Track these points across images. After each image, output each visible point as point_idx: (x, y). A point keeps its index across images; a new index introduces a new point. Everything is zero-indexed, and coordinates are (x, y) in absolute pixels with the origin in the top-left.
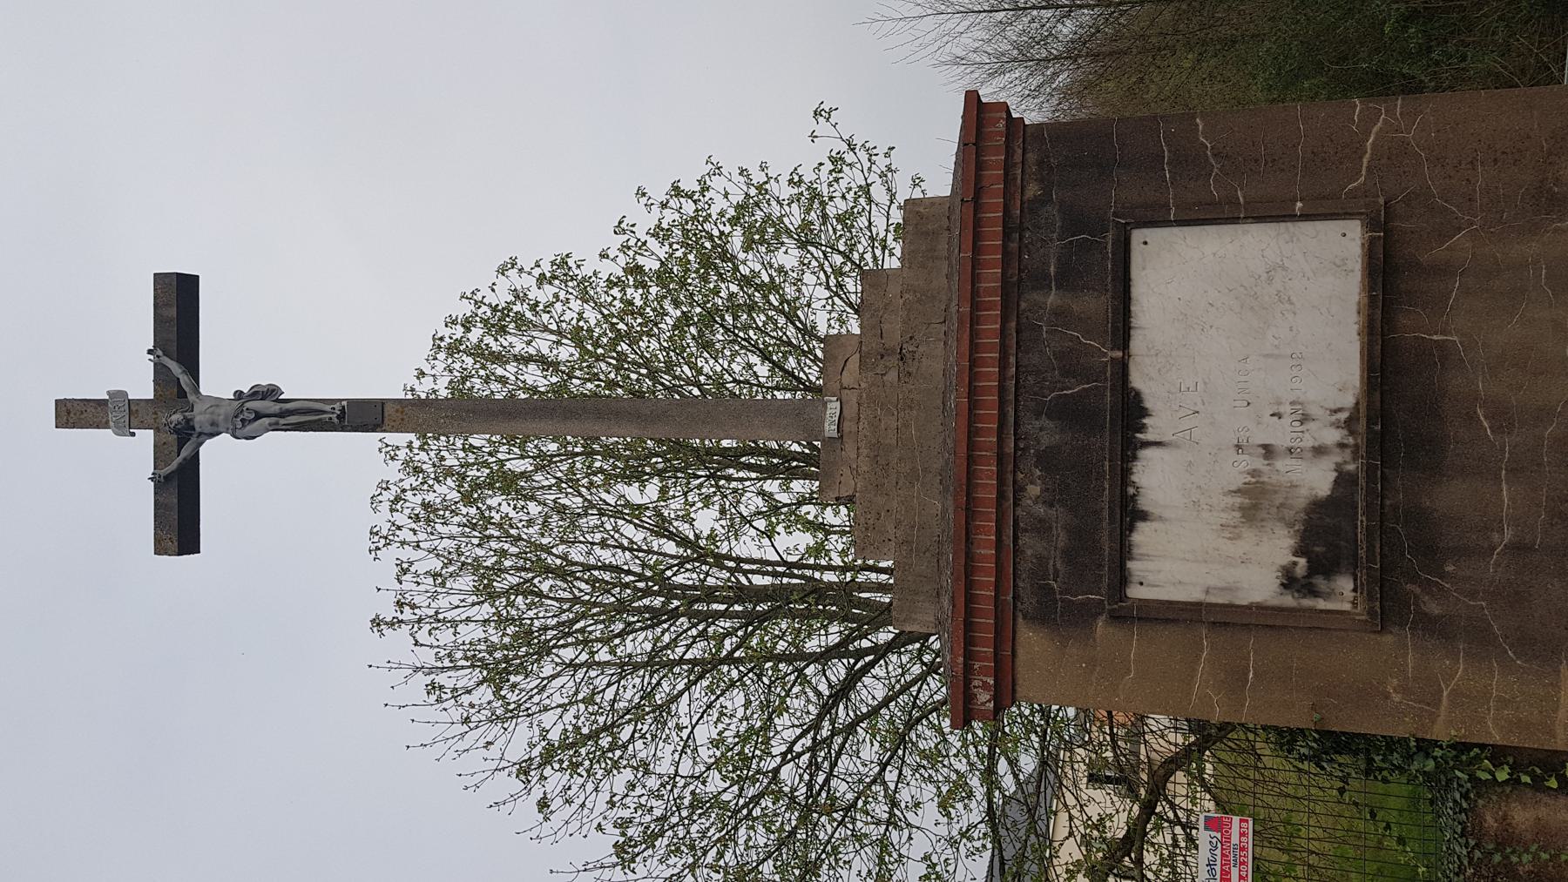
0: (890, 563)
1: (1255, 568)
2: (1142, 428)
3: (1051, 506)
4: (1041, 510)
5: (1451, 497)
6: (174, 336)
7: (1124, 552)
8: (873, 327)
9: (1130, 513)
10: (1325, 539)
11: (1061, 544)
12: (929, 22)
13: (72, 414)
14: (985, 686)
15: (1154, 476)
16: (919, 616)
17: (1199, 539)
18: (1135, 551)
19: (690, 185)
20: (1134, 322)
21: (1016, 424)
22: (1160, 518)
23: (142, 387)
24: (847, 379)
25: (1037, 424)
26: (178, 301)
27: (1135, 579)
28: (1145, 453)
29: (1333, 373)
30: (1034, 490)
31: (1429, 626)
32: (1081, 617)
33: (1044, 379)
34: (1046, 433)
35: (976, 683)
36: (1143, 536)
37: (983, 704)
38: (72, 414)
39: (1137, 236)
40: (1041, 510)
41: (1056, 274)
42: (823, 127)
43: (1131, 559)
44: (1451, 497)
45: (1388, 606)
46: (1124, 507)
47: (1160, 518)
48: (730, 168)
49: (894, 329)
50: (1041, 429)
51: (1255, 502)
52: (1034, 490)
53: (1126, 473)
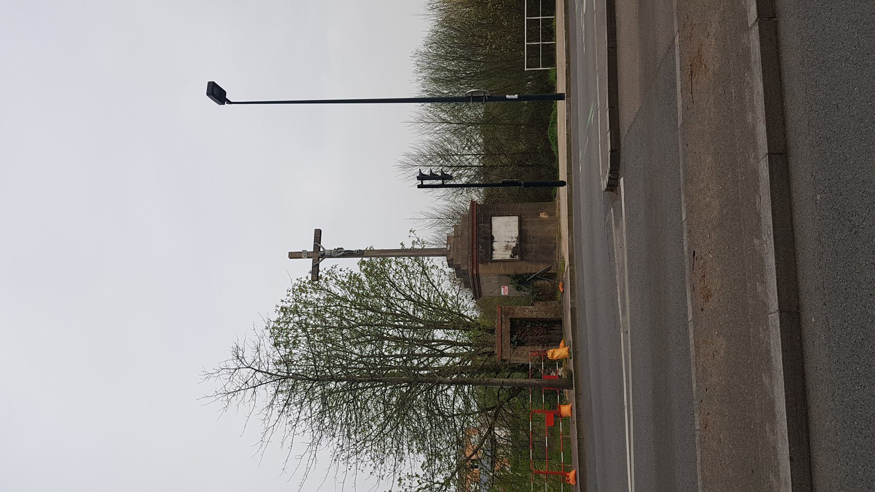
0: (516, 96)
1: (507, 255)
5: (529, 246)
7: (492, 254)
10: (515, 251)
12: (428, 221)
13: (293, 255)
15: (495, 245)
17: (500, 252)
23: (310, 249)
26: (318, 234)
29: (515, 233)
31: (526, 260)
32: (487, 262)
34: (482, 241)
36: (494, 252)
38: (293, 255)
44: (529, 246)
45: (522, 259)
49: (460, 233)
51: (507, 248)
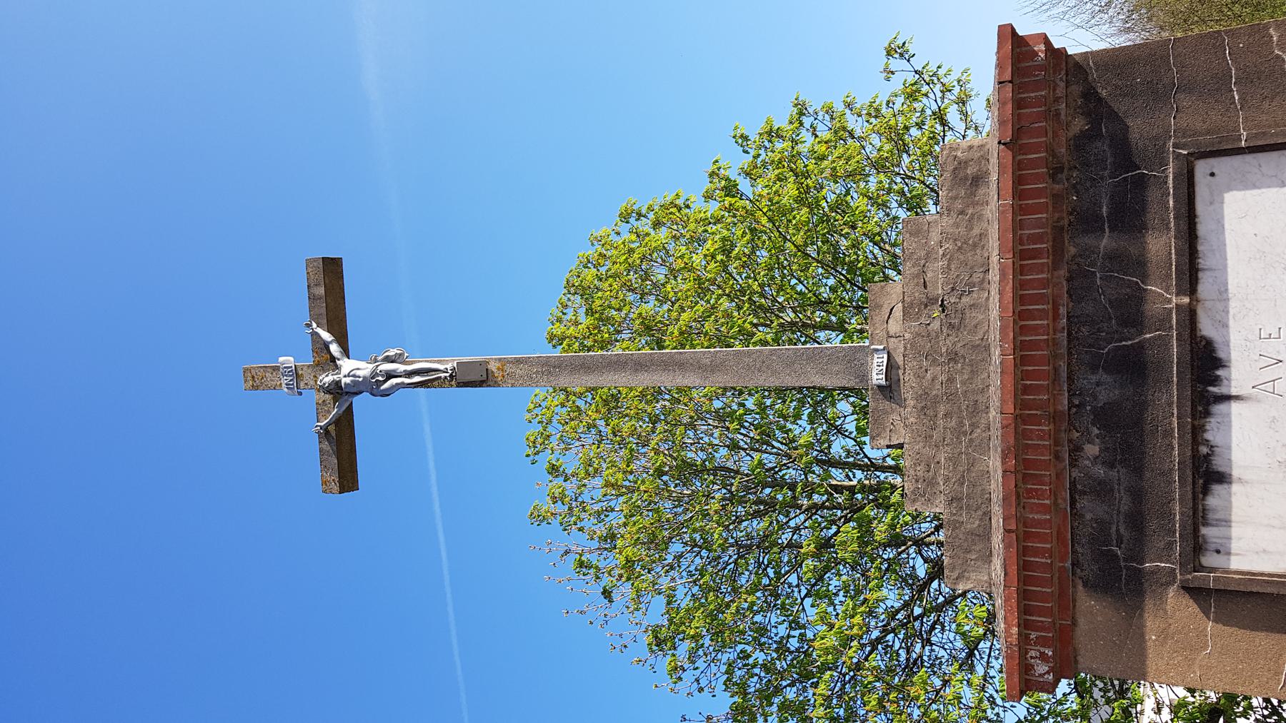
2: (1216, 381)
3: (1112, 466)
4: (1100, 471)
6: (323, 311)
7: (1198, 517)
8: (917, 276)
9: (1207, 474)
11: (1124, 508)
14: (1043, 657)
16: (973, 576)
18: (1211, 516)
19: (782, 123)
20: (1202, 263)
21: (1070, 379)
22: (1210, 270)
24: (894, 327)
25: (1094, 378)
27: (1213, 547)
28: (1219, 408)
30: (1092, 450)
33: (1099, 330)
35: (1033, 653)
37: (1041, 675)
39: (1202, 168)
40: (1100, 471)
41: (1110, 214)
42: (896, 64)
43: (1206, 524)
46: (1196, 469)
47: (1210, 270)
48: (814, 104)
50: (1098, 384)
52: (1092, 450)
53: (1196, 434)
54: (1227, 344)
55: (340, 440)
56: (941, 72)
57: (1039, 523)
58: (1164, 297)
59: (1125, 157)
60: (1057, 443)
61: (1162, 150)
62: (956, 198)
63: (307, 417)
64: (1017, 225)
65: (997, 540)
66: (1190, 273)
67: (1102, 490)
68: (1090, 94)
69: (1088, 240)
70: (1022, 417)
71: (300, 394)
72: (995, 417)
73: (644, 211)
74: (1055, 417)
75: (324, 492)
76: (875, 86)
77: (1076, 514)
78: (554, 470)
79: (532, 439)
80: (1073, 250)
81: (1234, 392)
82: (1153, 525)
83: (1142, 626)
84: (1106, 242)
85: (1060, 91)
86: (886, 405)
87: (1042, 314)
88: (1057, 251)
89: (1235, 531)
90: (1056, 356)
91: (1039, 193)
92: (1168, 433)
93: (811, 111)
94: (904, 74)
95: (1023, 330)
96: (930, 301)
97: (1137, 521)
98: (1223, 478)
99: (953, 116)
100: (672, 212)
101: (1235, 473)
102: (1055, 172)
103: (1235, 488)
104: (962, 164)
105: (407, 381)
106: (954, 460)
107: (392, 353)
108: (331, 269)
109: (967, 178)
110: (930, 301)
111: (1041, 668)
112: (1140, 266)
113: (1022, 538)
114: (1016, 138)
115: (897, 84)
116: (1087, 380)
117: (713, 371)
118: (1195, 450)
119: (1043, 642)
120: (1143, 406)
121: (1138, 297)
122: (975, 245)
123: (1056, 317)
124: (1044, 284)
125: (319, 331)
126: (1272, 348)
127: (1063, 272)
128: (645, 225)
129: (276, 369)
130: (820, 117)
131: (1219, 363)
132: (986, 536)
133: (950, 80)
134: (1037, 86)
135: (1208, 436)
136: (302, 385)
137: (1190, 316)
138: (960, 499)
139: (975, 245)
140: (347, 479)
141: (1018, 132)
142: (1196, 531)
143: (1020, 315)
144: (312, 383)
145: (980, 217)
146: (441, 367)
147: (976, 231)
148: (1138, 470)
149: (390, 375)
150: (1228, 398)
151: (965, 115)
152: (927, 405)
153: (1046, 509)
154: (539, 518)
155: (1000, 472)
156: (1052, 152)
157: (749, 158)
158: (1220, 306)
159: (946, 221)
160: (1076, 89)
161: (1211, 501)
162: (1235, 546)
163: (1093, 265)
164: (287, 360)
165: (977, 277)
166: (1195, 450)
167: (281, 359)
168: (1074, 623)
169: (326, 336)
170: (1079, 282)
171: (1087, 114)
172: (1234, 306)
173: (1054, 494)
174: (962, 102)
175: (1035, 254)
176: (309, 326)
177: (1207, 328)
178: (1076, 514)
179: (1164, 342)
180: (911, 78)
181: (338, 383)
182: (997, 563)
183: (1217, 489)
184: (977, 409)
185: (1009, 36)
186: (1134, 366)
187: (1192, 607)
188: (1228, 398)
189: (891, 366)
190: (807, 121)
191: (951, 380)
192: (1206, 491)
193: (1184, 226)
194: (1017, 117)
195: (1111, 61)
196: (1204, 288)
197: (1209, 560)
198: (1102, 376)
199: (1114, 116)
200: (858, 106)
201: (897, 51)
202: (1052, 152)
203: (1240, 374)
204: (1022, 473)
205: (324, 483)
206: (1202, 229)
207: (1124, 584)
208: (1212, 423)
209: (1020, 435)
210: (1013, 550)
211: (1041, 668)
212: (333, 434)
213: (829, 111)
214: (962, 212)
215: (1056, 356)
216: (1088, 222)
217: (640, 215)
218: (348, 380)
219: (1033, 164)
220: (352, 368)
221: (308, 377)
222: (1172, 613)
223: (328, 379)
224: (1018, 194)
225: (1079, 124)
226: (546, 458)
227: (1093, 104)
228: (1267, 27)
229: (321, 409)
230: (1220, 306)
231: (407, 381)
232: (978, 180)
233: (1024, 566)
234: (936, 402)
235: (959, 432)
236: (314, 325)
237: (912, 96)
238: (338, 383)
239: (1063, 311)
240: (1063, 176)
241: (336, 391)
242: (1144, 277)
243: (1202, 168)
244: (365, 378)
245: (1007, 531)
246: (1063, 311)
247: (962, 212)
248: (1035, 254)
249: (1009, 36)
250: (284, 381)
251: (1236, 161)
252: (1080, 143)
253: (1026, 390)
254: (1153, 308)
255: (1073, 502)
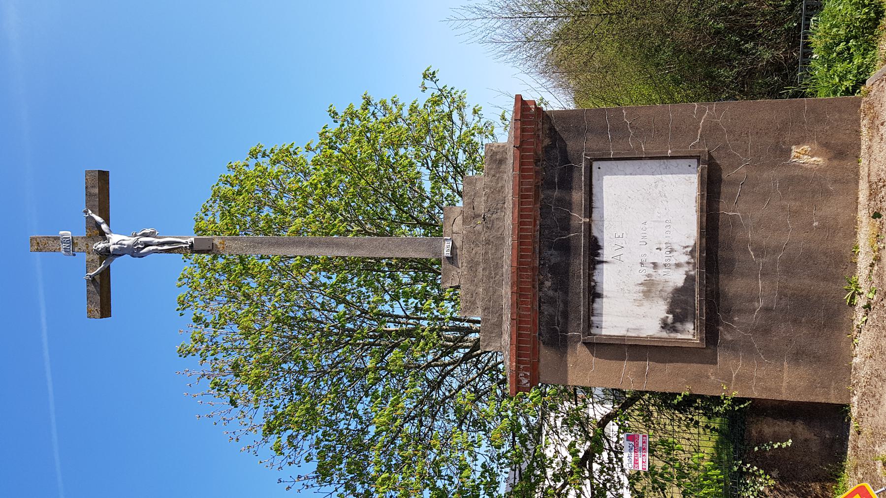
2: (598, 255)
3: (556, 291)
4: (551, 293)
6: (97, 203)
7: (590, 312)
9: (594, 294)
11: (561, 309)
16: (493, 344)
20: (594, 205)
24: (455, 229)
25: (550, 252)
28: (599, 266)
30: (548, 284)
39: (595, 165)
40: (551, 293)
42: (428, 83)
43: (593, 316)
46: (589, 292)
48: (375, 100)
52: (548, 284)
53: (590, 277)
54: (603, 239)
55: (101, 286)
56: (453, 92)
57: (525, 316)
58: (578, 218)
59: (565, 158)
60: (533, 281)
61: (580, 156)
62: (491, 169)
63: (78, 271)
64: (521, 183)
65: (507, 326)
66: (589, 209)
67: (552, 301)
68: (552, 129)
69: (549, 192)
70: (520, 268)
71: (74, 255)
72: (507, 270)
73: (268, 152)
74: (533, 269)
75: (89, 317)
76: (412, 94)
77: (541, 313)
78: (197, 319)
79: (182, 299)
80: (543, 196)
81: (605, 259)
82: (572, 316)
83: (566, 361)
84: (556, 193)
85: (540, 126)
86: (450, 266)
87: (529, 223)
88: (537, 196)
89: (604, 318)
90: (534, 242)
91: (530, 170)
92: (579, 277)
93: (373, 103)
94: (432, 89)
95: (521, 230)
96: (477, 216)
97: (565, 315)
98: (600, 296)
99: (455, 116)
100: (286, 156)
101: (605, 294)
102: (537, 161)
103: (604, 300)
104: (495, 154)
105: (160, 248)
106: (486, 290)
107: (148, 231)
108: (103, 177)
109: (496, 158)
110: (477, 216)
111: (525, 381)
112: (569, 204)
113: (518, 322)
114: (522, 144)
115: (427, 95)
116: (547, 253)
117: (355, 249)
118: (589, 284)
119: (526, 369)
120: (568, 265)
121: (568, 217)
122: (499, 191)
123: (535, 225)
124: (531, 210)
125: (93, 215)
126: (620, 242)
127: (538, 205)
128: (265, 162)
129: (58, 238)
130: (379, 107)
131: (600, 248)
132: (499, 325)
133: (456, 97)
134: (530, 123)
135: (594, 278)
136: (76, 249)
137: (589, 227)
138: (489, 309)
139: (499, 191)
140: (105, 311)
141: (522, 143)
142: (589, 318)
143: (521, 223)
144: (84, 248)
145: (502, 178)
146: (184, 241)
147: (500, 185)
148: (566, 293)
149: (147, 245)
150: (603, 262)
151: (462, 117)
152: (473, 266)
153: (528, 310)
154: (185, 353)
155: (509, 293)
156: (536, 153)
157: (338, 126)
158: (600, 223)
159: (487, 179)
160: (546, 126)
161: (595, 306)
162: (604, 325)
163: (551, 203)
164: (67, 233)
165: (499, 206)
166: (589, 284)
167: (61, 232)
168: (539, 361)
169: (98, 219)
170: (545, 210)
171: (551, 137)
172: (606, 223)
173: (532, 303)
174: (459, 108)
175: (527, 197)
176: (86, 212)
177: (595, 233)
178: (541, 313)
179: (579, 237)
180: (437, 93)
181: (107, 249)
182: (506, 337)
183: (597, 300)
184: (498, 266)
185: (519, 99)
186: (566, 248)
187: (587, 352)
188: (603, 262)
189: (454, 247)
190: (372, 109)
191: (486, 253)
192: (593, 302)
193: (588, 189)
194: (522, 136)
195: (563, 115)
196: (595, 215)
197: (594, 331)
198: (553, 252)
199: (561, 139)
200: (400, 104)
201: (430, 75)
202: (536, 153)
203: (607, 253)
204: (519, 293)
205: (89, 311)
206: (594, 191)
207: (559, 342)
208: (596, 272)
209: (519, 276)
210: (515, 328)
211: (525, 381)
212: (98, 281)
213: (384, 105)
214: (494, 176)
215: (534, 242)
216: (549, 184)
217: (264, 155)
218: (116, 247)
219: (528, 157)
220: (115, 239)
221: (82, 245)
222: (579, 355)
223: (101, 245)
224: (522, 170)
225: (547, 142)
226: (190, 314)
227: (553, 133)
228: (622, 109)
229: (89, 265)
230: (600, 223)
231: (160, 248)
232: (501, 161)
233: (519, 335)
234: (477, 264)
235: (489, 277)
236: (90, 212)
237: (436, 103)
238: (107, 249)
239: (538, 222)
240: (539, 163)
241: (106, 254)
242: (571, 210)
243: (595, 165)
244: (128, 246)
245: (512, 319)
246: (538, 222)
247: (494, 176)
248: (527, 197)
249: (519, 99)
250: (63, 246)
251: (609, 163)
252: (547, 149)
253: (522, 257)
254: (574, 223)
255: (540, 307)
